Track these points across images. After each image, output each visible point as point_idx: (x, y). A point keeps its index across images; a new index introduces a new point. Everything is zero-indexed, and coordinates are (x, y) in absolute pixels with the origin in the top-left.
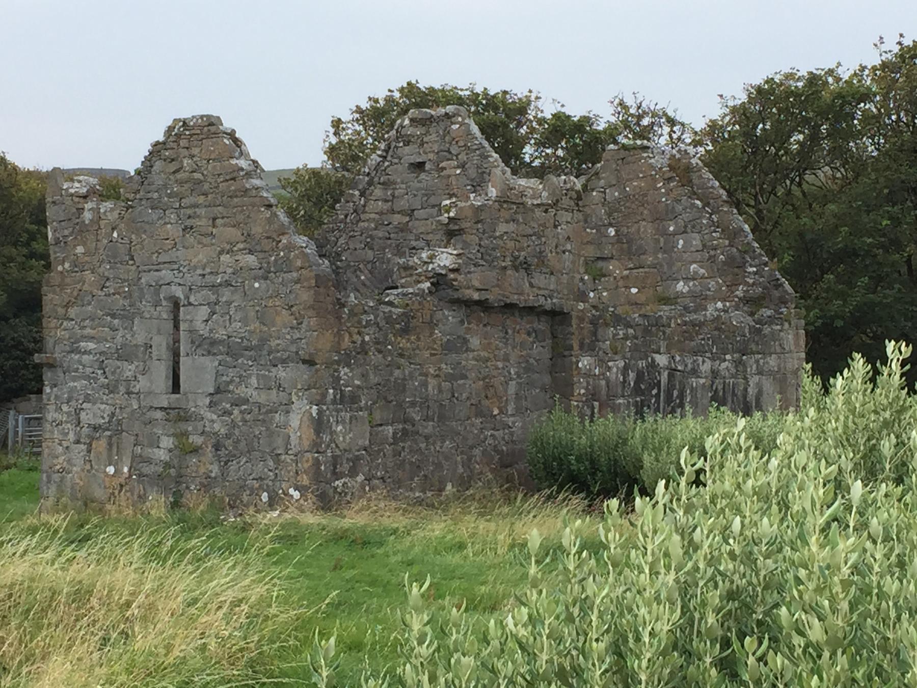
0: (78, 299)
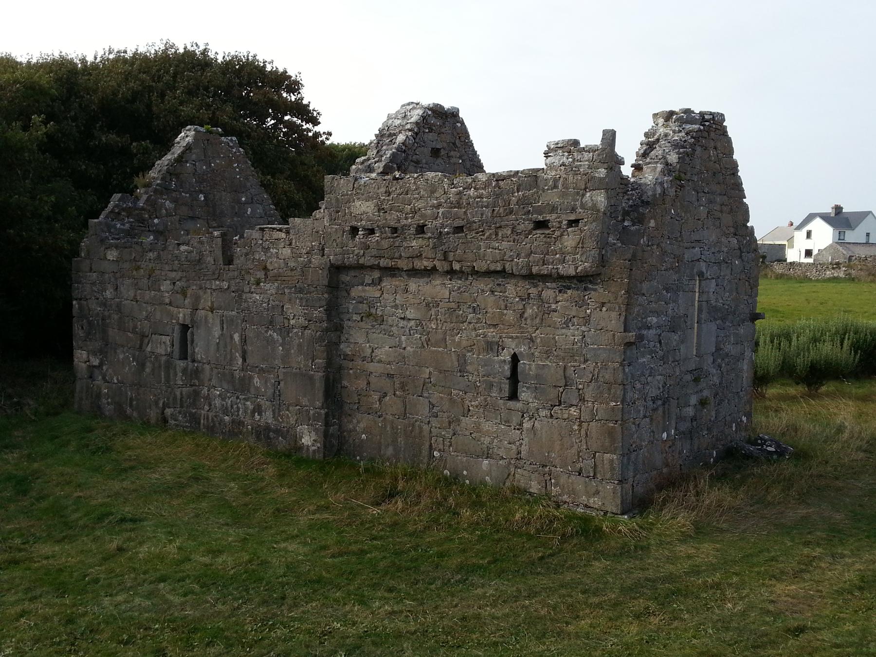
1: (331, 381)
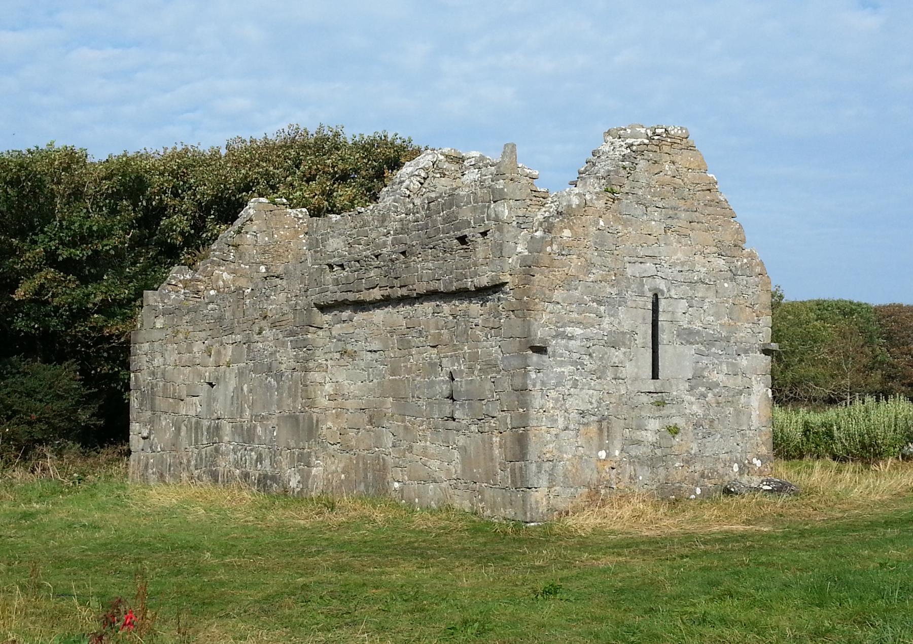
0: (568, 282)
1: (315, 421)
